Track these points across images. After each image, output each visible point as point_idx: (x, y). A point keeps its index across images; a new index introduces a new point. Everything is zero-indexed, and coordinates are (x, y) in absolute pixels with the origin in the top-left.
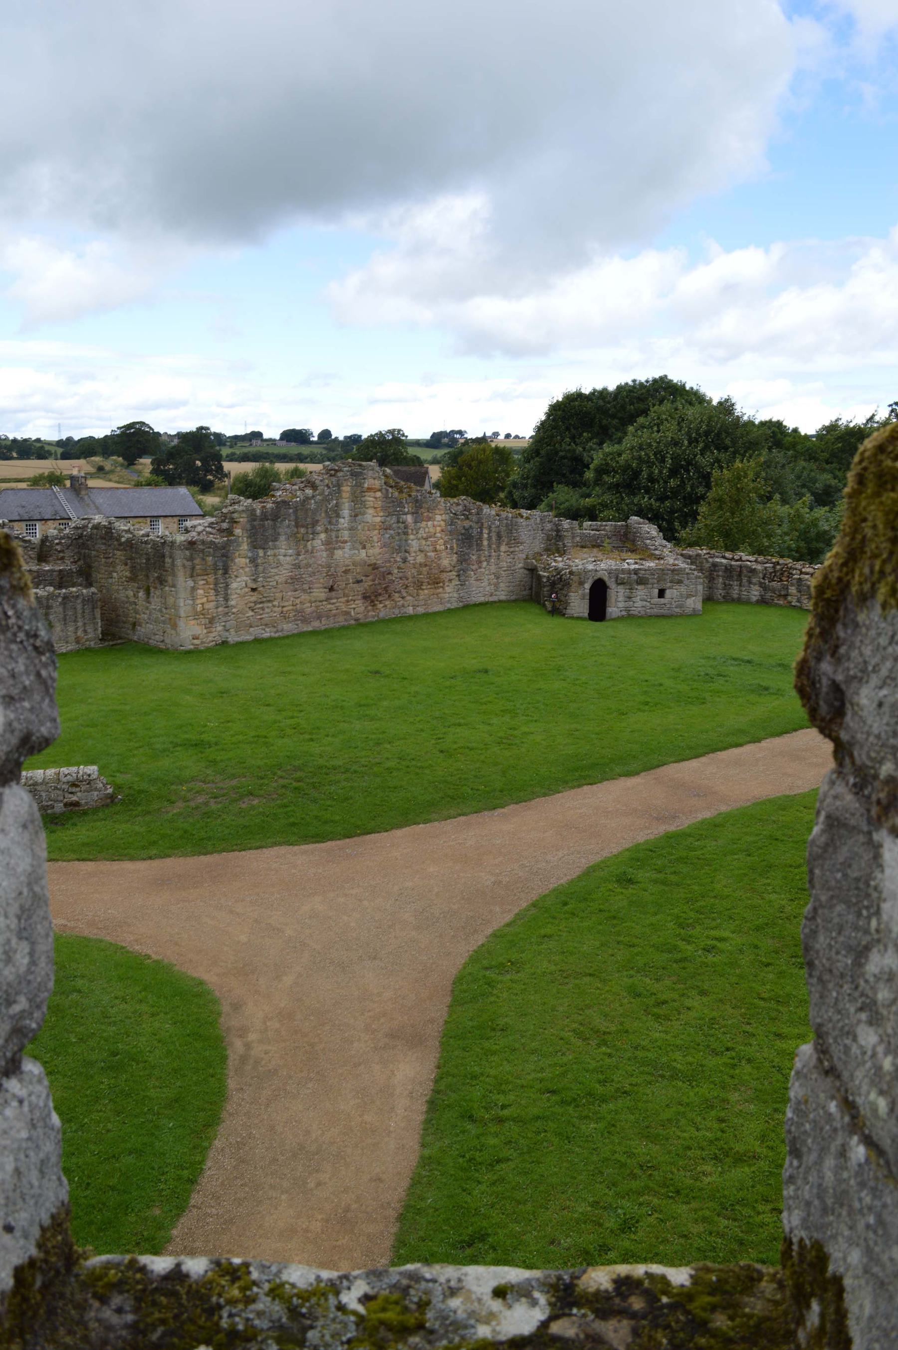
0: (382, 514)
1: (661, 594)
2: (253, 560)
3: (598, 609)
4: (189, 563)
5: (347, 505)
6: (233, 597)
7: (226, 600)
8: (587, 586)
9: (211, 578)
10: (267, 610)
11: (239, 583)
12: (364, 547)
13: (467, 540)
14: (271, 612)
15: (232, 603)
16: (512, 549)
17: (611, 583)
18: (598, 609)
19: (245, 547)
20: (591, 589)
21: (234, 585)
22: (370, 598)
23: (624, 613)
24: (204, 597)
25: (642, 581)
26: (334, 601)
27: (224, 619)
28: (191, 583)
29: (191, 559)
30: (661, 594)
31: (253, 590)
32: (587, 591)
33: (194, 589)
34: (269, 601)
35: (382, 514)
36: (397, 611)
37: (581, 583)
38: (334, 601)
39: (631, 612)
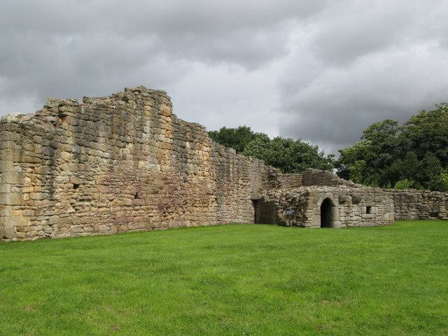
0: (171, 136)
1: (368, 211)
2: (77, 155)
3: (326, 220)
4: (18, 147)
5: (148, 122)
6: (57, 190)
7: (52, 193)
8: (319, 204)
9: (38, 168)
10: (87, 209)
11: (64, 176)
12: (160, 163)
13: (222, 171)
14: (89, 210)
15: (56, 196)
16: (244, 184)
17: (336, 202)
18: (326, 220)
19: (70, 141)
20: (322, 207)
21: (59, 178)
22: (163, 209)
23: (344, 225)
24: (32, 189)
25: (356, 201)
26: (138, 207)
27: (48, 213)
28: (19, 168)
29: (19, 143)
30: (368, 211)
31: (76, 186)
32: (319, 208)
33: (21, 176)
34: (89, 200)
35: (171, 136)
36: (180, 223)
37: (315, 202)
38: (138, 207)
39: (349, 225)
